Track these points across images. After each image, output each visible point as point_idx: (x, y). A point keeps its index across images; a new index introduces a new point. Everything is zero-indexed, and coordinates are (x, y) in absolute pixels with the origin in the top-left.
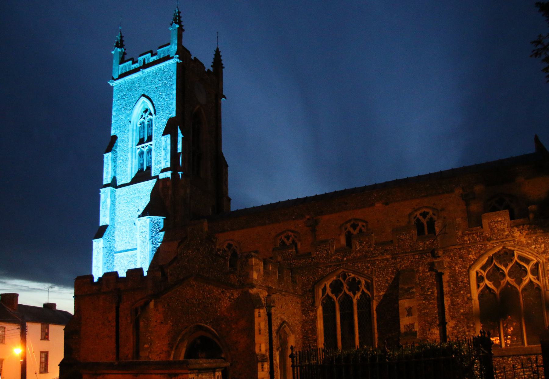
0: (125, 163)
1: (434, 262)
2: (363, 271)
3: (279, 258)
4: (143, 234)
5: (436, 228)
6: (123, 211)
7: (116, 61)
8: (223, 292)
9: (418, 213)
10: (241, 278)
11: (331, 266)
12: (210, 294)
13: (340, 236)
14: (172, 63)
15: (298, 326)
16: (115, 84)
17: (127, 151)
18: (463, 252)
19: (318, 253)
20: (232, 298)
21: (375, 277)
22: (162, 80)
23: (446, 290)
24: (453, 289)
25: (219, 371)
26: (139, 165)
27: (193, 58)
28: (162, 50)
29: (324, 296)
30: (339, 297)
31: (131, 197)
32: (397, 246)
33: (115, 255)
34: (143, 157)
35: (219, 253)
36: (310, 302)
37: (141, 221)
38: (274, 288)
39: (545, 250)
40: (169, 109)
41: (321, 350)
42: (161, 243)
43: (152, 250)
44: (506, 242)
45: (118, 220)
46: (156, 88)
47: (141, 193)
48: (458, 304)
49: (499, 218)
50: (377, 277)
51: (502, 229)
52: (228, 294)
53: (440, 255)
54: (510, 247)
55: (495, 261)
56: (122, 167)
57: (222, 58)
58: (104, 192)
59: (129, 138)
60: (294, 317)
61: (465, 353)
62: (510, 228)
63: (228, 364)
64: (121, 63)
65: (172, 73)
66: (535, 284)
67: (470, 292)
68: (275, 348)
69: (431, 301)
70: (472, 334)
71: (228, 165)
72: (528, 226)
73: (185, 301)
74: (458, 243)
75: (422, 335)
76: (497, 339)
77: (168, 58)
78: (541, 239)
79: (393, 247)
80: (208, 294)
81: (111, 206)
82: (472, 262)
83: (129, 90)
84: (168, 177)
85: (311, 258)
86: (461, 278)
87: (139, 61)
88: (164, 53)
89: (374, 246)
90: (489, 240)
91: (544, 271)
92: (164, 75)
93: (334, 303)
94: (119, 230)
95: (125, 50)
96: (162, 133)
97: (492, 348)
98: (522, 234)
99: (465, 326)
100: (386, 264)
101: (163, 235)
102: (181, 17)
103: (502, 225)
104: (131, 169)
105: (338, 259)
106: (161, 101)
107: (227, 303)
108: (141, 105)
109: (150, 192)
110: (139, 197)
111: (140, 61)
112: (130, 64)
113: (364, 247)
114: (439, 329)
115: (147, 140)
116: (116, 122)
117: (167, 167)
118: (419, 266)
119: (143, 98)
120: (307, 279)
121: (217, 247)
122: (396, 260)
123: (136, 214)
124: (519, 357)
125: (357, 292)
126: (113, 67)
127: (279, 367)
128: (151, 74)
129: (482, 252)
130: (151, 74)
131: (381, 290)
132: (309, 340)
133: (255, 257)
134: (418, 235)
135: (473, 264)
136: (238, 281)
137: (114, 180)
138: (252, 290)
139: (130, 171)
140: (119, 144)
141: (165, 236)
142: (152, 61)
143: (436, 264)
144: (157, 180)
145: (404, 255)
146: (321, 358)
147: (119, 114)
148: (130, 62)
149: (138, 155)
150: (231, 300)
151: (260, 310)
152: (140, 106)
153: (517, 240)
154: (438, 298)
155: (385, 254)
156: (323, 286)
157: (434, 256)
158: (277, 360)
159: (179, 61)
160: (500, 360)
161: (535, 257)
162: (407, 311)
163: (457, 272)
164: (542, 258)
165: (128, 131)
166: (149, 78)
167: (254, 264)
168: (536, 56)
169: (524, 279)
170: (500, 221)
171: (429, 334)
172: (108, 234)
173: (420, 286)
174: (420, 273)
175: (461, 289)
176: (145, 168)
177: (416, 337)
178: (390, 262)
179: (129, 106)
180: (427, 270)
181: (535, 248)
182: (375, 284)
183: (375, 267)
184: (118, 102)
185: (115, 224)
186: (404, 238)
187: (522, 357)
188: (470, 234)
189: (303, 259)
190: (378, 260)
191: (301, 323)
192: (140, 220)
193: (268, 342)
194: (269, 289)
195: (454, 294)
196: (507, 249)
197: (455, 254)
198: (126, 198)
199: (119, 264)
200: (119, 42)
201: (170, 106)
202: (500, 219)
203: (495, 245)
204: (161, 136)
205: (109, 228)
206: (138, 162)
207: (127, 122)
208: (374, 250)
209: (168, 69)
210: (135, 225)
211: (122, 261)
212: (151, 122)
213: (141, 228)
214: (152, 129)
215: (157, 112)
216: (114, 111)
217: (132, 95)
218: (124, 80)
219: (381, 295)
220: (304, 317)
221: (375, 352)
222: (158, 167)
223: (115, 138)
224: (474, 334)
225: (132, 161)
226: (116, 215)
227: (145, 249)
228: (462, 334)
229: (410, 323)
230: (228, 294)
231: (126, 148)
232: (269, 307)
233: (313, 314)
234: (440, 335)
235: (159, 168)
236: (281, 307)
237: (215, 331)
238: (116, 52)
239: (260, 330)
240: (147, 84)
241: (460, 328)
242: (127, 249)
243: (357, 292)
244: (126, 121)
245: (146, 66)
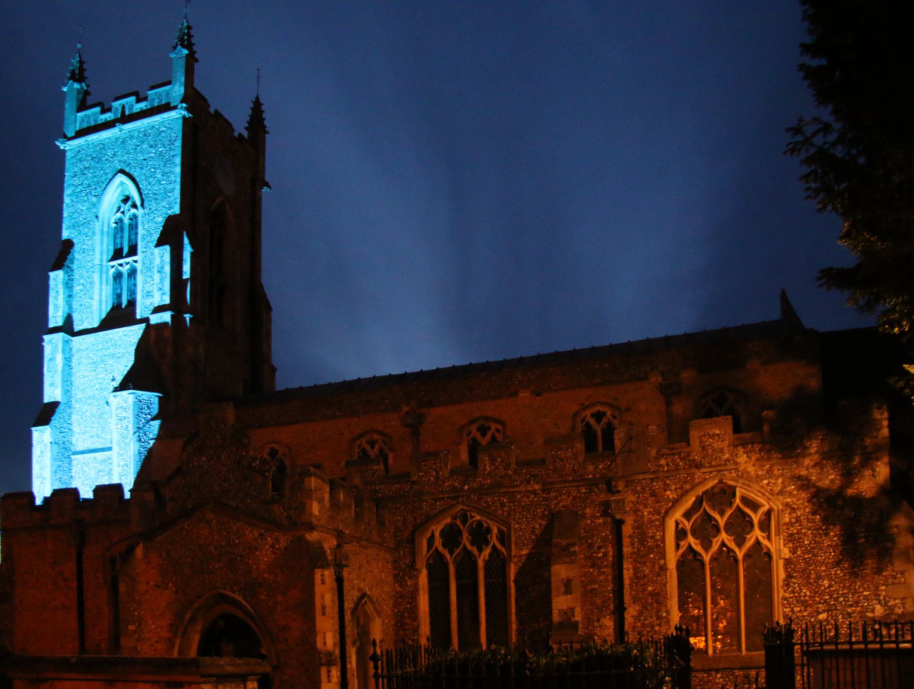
0: (88, 291)
1: (609, 501)
2: (496, 511)
3: (357, 481)
4: (122, 423)
5: (615, 441)
6: (86, 379)
7: (70, 106)
8: (261, 535)
9: (588, 413)
10: (292, 512)
11: (443, 498)
12: (238, 538)
13: (460, 447)
14: (175, 117)
15: (387, 603)
16: (69, 147)
17: (92, 270)
18: (657, 485)
19: (421, 474)
20: (277, 547)
21: (514, 522)
22: (156, 146)
23: (627, 552)
24: (638, 550)
25: (252, 680)
27: (212, 110)
28: (156, 93)
29: (431, 552)
30: (455, 554)
31: (100, 354)
32: (552, 470)
33: (73, 457)
35: (254, 464)
36: (408, 561)
37: (118, 399)
38: (347, 532)
39: (782, 489)
40: (168, 199)
41: (423, 648)
42: (154, 441)
43: (139, 453)
44: (725, 473)
45: (77, 394)
46: (145, 160)
48: (645, 576)
49: (716, 430)
50: (518, 523)
51: (720, 449)
52: (269, 539)
53: (620, 489)
54: (731, 480)
55: (706, 503)
57: (264, 115)
59: (95, 246)
60: (381, 588)
61: (650, 665)
62: (732, 448)
63: (268, 669)
64: (80, 110)
65: (174, 135)
66: (764, 546)
67: (663, 555)
68: (349, 641)
69: (602, 570)
70: (663, 630)
72: (760, 446)
73: (197, 548)
74: (649, 469)
75: (586, 629)
76: (702, 641)
77: (166, 108)
78: (778, 470)
79: (545, 471)
80: (235, 537)
81: (63, 367)
82: (671, 504)
83: (97, 159)
84: (166, 321)
85: (409, 483)
86: (651, 531)
87: (113, 109)
88: (160, 98)
89: (515, 466)
90: (699, 466)
91: (778, 524)
92: (160, 138)
93: (446, 565)
94: (80, 413)
95: (88, 86)
96: (155, 242)
97: (691, 657)
98: (750, 458)
99: (654, 616)
100: (533, 499)
102: (192, 36)
103: (720, 443)
104: (99, 303)
105: (454, 487)
106: (154, 184)
107: (269, 556)
108: (117, 187)
109: (134, 347)
110: (114, 354)
111: (116, 108)
112: (96, 113)
113: (497, 468)
114: (613, 619)
115: (128, 252)
116: (70, 216)
117: (164, 303)
118: (586, 507)
120: (403, 519)
121: (251, 453)
122: (549, 493)
124: (733, 673)
125: (484, 546)
126: (66, 116)
127: (356, 674)
128: (136, 134)
129: (687, 487)
130: (136, 134)
131: (524, 545)
132: (405, 630)
133: (315, 474)
134: (586, 452)
135: (670, 508)
136: (287, 517)
137: (69, 320)
138: (311, 534)
139: (98, 307)
140: (76, 257)
141: (161, 427)
142: (138, 110)
143: (613, 505)
145: (563, 485)
146: (423, 664)
147: (77, 202)
148: (98, 109)
149: (111, 279)
150: (275, 551)
151: (323, 571)
152: (115, 191)
153: (742, 470)
154: (613, 564)
155: (532, 482)
156: (429, 534)
157: (611, 490)
158: (353, 663)
159: (186, 114)
160: (703, 677)
161: (766, 501)
162: (565, 585)
163: (646, 519)
164: (778, 503)
165: (94, 233)
166: (132, 141)
167: (313, 488)
168: (792, 154)
169: (749, 537)
170: (718, 435)
171: (596, 627)
172: (60, 418)
173: (586, 541)
174: (587, 519)
175: (650, 550)
177: (577, 631)
178: (540, 497)
179: (96, 189)
180: (599, 515)
181: (768, 484)
182: (515, 534)
183: (514, 505)
184: (75, 180)
185: (71, 401)
186: (563, 455)
187: (737, 673)
188: (670, 455)
189: (397, 483)
190: (520, 492)
191: (392, 598)
192: (116, 396)
193: (338, 630)
194: (339, 534)
195: (639, 558)
196: (726, 484)
197: (643, 489)
198: (90, 355)
199: (81, 475)
200: (77, 72)
201: (170, 194)
202: (717, 432)
203: (707, 477)
205: (61, 407)
206: (112, 292)
207: (90, 216)
208: (514, 474)
209: (166, 127)
210: (108, 405)
211: (86, 469)
212: (135, 220)
213: (118, 411)
214: (136, 234)
215: (145, 203)
216: (67, 196)
217: (101, 170)
218: (86, 141)
219: (524, 555)
220: (398, 588)
221: (509, 657)
222: (148, 302)
223: (69, 244)
224: (667, 630)
225: (101, 289)
227: (125, 449)
228: (648, 629)
229: (568, 607)
230: (269, 539)
232: (339, 567)
233: (413, 582)
234: (614, 629)
236: (360, 568)
237: (249, 607)
238: (71, 88)
239: (324, 608)
240: (128, 151)
241: (645, 619)
243: (484, 546)
244: (89, 216)
245: (126, 118)
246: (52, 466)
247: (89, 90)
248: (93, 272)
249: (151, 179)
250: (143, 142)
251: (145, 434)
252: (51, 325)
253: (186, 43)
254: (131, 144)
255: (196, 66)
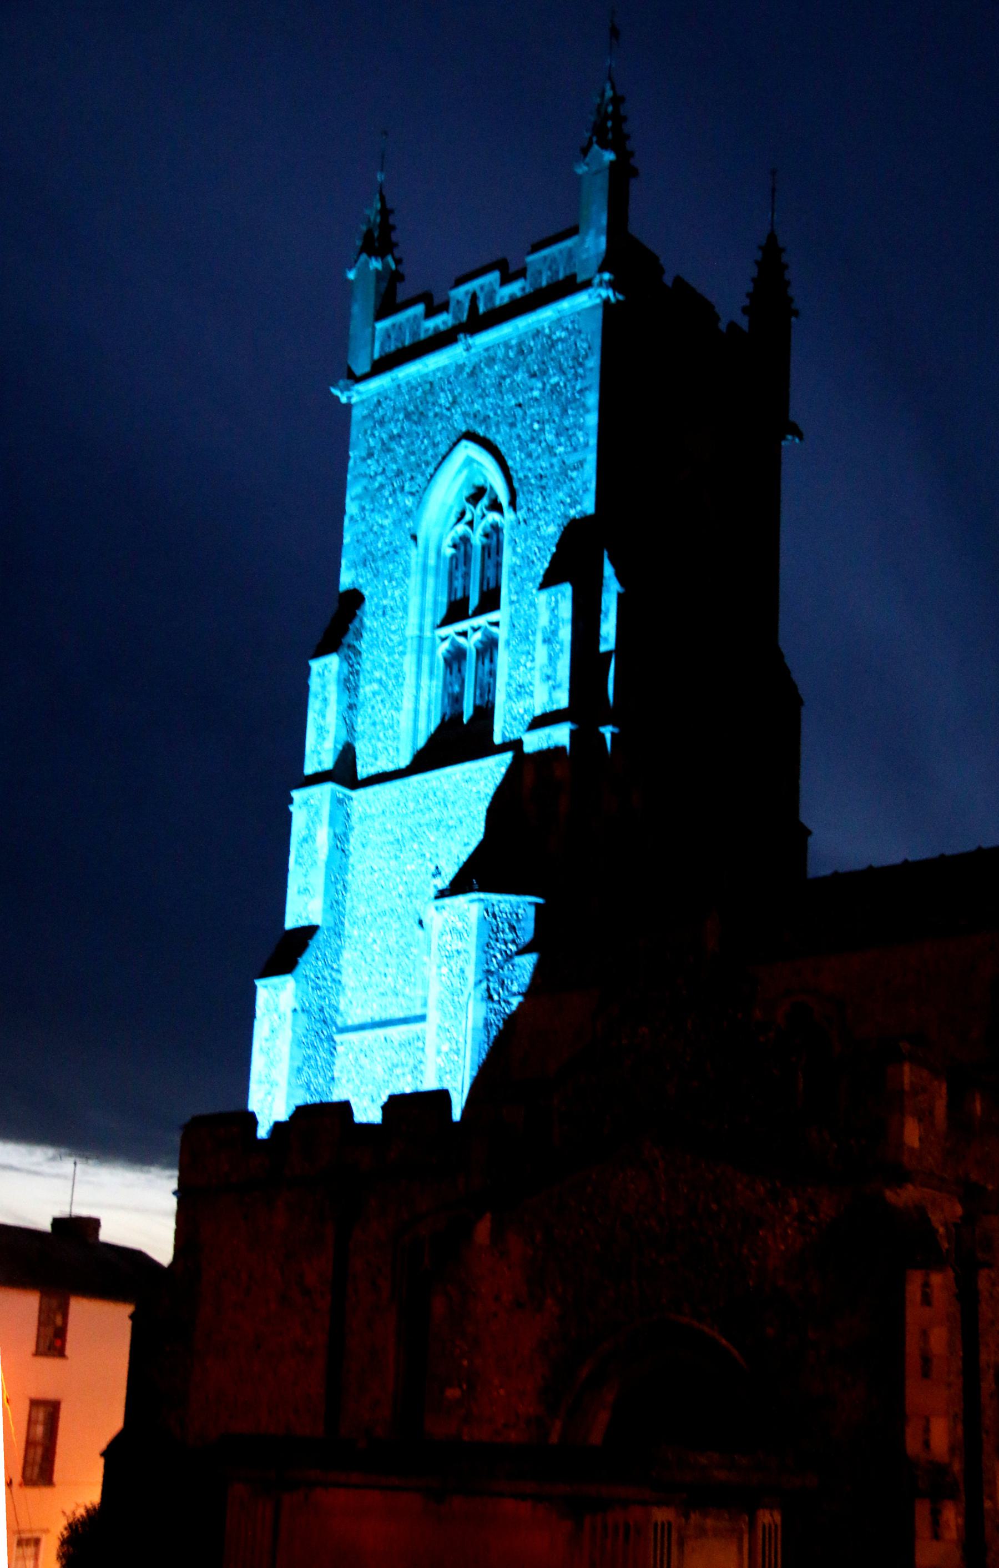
0: (390, 694)
4: (452, 963)
7: (361, 308)
26: (446, 700)
28: (545, 258)
31: (410, 822)
34: (462, 668)
37: (445, 913)
42: (520, 999)
45: (356, 906)
46: (520, 405)
47: (449, 806)
52: (794, 1202)
56: (377, 709)
58: (306, 803)
64: (380, 315)
71: (804, 698)
83: (417, 415)
88: (554, 267)
95: (398, 261)
96: (540, 580)
101: (530, 968)
108: (460, 471)
109: (486, 804)
111: (458, 302)
112: (415, 317)
117: (555, 707)
119: (466, 447)
123: (428, 886)
126: (352, 331)
128: (500, 353)
130: (500, 353)
137: (347, 756)
139: (411, 724)
142: (506, 300)
144: (514, 758)
148: (419, 309)
152: (455, 478)
165: (406, 573)
167: (907, 1087)
176: (468, 711)
200: (376, 234)
201: (574, 474)
204: (534, 591)
205: (320, 937)
206: (440, 691)
207: (401, 538)
214: (498, 565)
215: (520, 500)
222: (520, 707)
223: (355, 599)
226: (348, 888)
230: (794, 1202)
231: (396, 638)
235: (525, 711)
242: (386, 1016)
246: (292, 1058)
247: (401, 269)
248: (402, 654)
249: (532, 446)
250: (515, 369)
251: (502, 984)
252: (310, 768)
253: (610, 136)
254: (489, 375)
255: (635, 187)
